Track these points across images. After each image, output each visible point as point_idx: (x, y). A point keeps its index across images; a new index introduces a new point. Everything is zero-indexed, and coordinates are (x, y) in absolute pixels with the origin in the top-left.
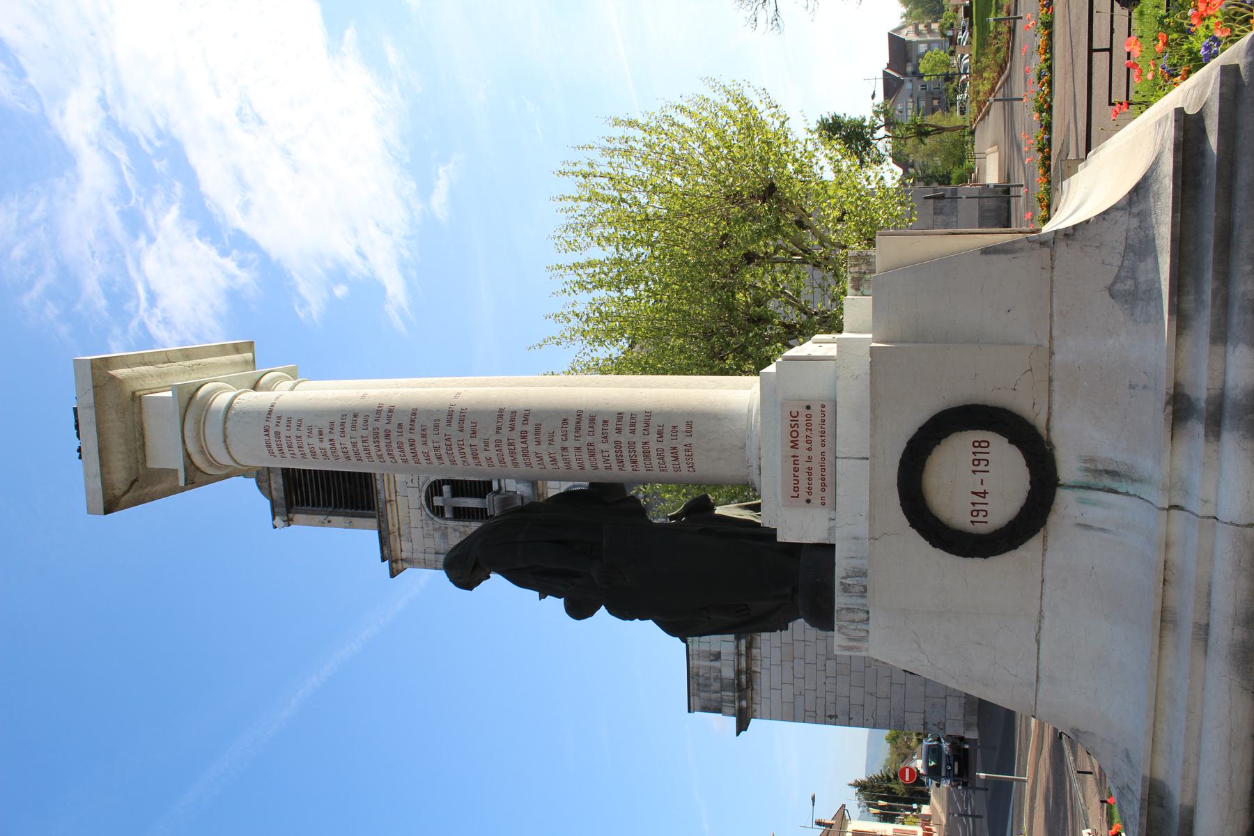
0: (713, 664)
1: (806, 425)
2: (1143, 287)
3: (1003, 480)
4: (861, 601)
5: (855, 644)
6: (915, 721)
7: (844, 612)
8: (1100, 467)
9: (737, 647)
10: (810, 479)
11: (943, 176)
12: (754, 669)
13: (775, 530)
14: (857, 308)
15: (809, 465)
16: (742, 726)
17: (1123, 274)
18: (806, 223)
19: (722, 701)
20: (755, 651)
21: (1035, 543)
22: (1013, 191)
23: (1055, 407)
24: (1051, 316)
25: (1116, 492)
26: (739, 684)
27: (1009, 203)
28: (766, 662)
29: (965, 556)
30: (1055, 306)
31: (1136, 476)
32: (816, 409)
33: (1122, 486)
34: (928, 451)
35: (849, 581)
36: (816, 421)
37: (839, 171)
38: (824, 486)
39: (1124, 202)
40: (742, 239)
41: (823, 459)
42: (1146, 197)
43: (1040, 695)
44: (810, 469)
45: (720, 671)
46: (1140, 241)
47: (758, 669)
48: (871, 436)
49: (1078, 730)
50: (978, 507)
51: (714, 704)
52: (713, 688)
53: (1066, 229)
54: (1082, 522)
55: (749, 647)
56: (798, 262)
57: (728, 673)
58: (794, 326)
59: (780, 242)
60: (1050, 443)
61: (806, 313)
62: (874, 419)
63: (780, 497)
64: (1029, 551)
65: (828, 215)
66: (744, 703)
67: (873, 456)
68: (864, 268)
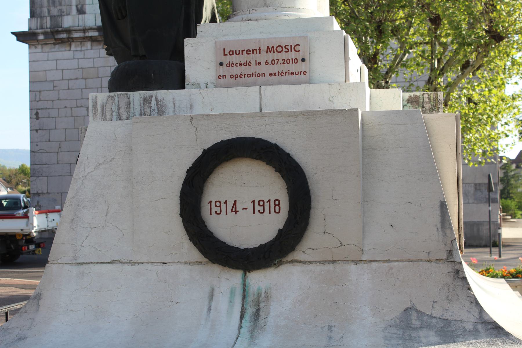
0: (74, 8)
1: (287, 58)
2: (414, 334)
3: (248, 227)
4: (137, 113)
5: (99, 110)
6: (40, 185)
7: (126, 100)
8: (262, 305)
9: (91, 29)
10: (240, 64)
11: (509, 193)
12: (73, 45)
13: (194, 36)
14: (393, 99)
15: (253, 63)
16: (21, 36)
17: (425, 318)
18: (466, 71)
19: (42, 17)
20: (88, 44)
21: (196, 255)
22: (495, 250)
23: (311, 267)
24: (388, 261)
25: (242, 318)
26: (58, 32)
27: (485, 246)
28: (80, 55)
29: (181, 198)
30: (396, 264)
31: (256, 333)
32: (302, 67)
33: (246, 323)
34: (269, 162)
35: (154, 102)
36: (292, 67)
37: (514, 99)
38: (235, 77)
39: (486, 318)
40: (453, 13)
41: (259, 75)
42: (491, 335)
43: (65, 266)
44: (250, 64)
45: (68, 15)
46: (453, 331)
47: (73, 47)
48: (280, 113)
49: (40, 299)
50: (223, 206)
51: (38, 11)
52: (52, 8)
53: (463, 271)
54: (215, 293)
55: (92, 39)
56: (432, 65)
57: (67, 22)
58: (376, 63)
59: (450, 48)
60: (281, 263)
61: (387, 73)
62: (295, 115)
63: (224, 39)
64: (189, 250)
65: (474, 90)
66: (41, 37)
67: (263, 115)
68: (427, 106)
